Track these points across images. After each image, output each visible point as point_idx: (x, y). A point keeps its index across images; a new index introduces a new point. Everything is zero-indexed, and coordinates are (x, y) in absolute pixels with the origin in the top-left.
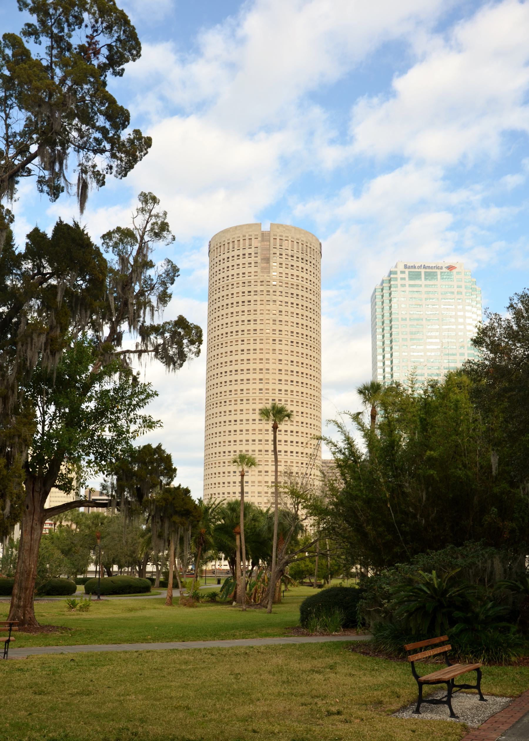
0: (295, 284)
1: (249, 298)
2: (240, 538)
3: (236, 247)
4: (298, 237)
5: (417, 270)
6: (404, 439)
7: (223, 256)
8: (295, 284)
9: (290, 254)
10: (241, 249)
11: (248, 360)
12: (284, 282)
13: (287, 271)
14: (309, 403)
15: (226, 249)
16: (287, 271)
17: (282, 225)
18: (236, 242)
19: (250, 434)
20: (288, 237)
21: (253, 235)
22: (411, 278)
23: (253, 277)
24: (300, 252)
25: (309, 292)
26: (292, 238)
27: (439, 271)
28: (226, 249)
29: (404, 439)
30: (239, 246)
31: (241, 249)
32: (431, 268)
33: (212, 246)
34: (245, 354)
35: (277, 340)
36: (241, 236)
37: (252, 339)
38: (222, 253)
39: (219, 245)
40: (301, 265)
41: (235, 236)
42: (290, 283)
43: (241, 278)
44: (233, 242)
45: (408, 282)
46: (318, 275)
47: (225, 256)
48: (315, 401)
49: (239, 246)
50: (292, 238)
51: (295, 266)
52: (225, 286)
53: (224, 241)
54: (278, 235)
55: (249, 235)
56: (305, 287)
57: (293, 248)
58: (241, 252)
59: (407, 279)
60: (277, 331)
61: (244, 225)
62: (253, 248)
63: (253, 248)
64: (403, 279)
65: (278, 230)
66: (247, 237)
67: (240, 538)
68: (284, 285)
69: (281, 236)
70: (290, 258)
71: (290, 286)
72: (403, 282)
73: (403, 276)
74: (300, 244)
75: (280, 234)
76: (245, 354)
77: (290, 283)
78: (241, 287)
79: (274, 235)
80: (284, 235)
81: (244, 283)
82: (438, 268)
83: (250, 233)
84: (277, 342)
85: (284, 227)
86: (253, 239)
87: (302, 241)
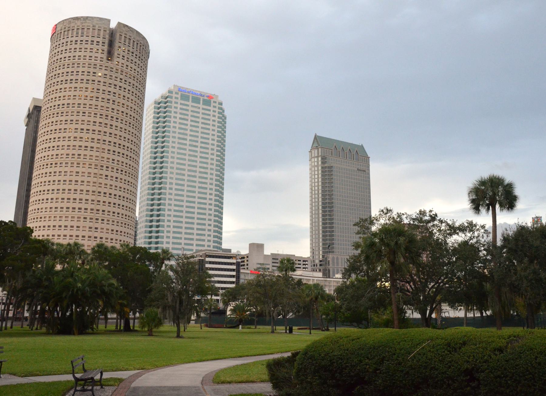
2: (210, 263)
5: (187, 94)
9: (131, 51)
14: (128, 172)
17: (127, 26)
19: (62, 184)
22: (182, 99)
24: (139, 51)
27: (202, 98)
31: (85, 36)
32: (197, 95)
33: (57, 29)
34: (74, 124)
35: (115, 117)
36: (92, 25)
37: (93, 113)
38: (62, 37)
39: (67, 29)
45: (179, 101)
47: (64, 41)
48: (133, 171)
52: (58, 66)
53: (74, 27)
54: (124, 33)
59: (179, 99)
61: (95, 18)
64: (176, 98)
65: (124, 29)
67: (210, 263)
68: (124, 74)
69: (125, 34)
70: (131, 54)
72: (176, 100)
73: (176, 96)
74: (139, 45)
75: (126, 32)
79: (120, 32)
80: (128, 34)
82: (201, 95)
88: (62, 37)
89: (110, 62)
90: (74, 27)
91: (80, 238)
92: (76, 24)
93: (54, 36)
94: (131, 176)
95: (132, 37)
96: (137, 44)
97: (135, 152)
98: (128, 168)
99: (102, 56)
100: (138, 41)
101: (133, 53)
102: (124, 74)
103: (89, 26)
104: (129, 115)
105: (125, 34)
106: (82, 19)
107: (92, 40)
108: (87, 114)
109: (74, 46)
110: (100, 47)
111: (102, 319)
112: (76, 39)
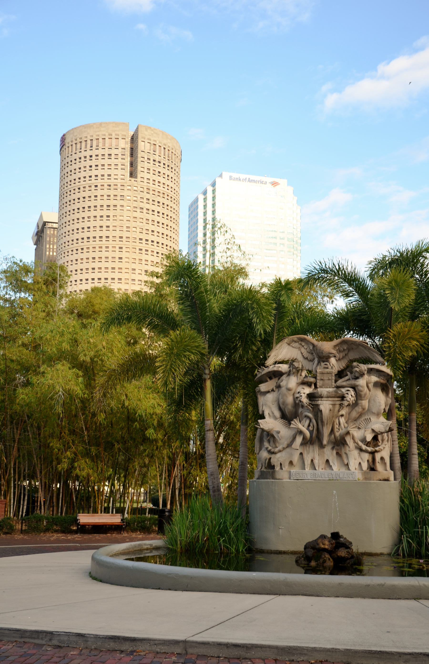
0: (162, 192)
1: (115, 202)
3: (101, 145)
4: (165, 142)
6: (342, 539)
7: (79, 155)
8: (162, 192)
9: (157, 160)
10: (107, 149)
11: (113, 268)
12: (151, 189)
13: (155, 177)
15: (89, 146)
16: (155, 177)
18: (101, 140)
20: (155, 141)
21: (120, 135)
23: (119, 180)
24: (167, 158)
25: (170, 180)
26: (160, 142)
28: (89, 146)
29: (342, 539)
30: (86, 147)
31: (107, 149)
36: (107, 134)
40: (167, 173)
41: (100, 133)
42: (157, 190)
43: (106, 180)
44: (86, 141)
46: (177, 170)
49: (86, 147)
50: (160, 142)
51: (162, 173)
53: (86, 137)
55: (116, 135)
56: (170, 195)
57: (160, 153)
58: (107, 152)
60: (144, 240)
62: (120, 149)
63: (120, 150)
65: (146, 133)
66: (114, 136)
68: (151, 192)
70: (157, 164)
71: (157, 194)
74: (167, 150)
75: (148, 137)
76: (110, 262)
77: (157, 190)
78: (106, 190)
79: (142, 138)
80: (152, 139)
81: (110, 185)
83: (117, 133)
84: (144, 252)
85: (152, 130)
86: (120, 139)
87: (169, 147)
88: (74, 151)
89: (133, 179)
90: (86, 137)
91: (109, 281)
92: (88, 134)
93: (62, 149)
94: (173, 221)
95: (158, 142)
96: (164, 148)
97: (172, 210)
98: (169, 191)
99: (123, 172)
100: (165, 145)
101: (159, 162)
102: (151, 192)
103: (105, 135)
104: (161, 204)
105: (149, 139)
106: (95, 126)
107: (110, 153)
108: (111, 249)
109: (88, 163)
110: (119, 161)
111: (138, 505)
112: (90, 153)
